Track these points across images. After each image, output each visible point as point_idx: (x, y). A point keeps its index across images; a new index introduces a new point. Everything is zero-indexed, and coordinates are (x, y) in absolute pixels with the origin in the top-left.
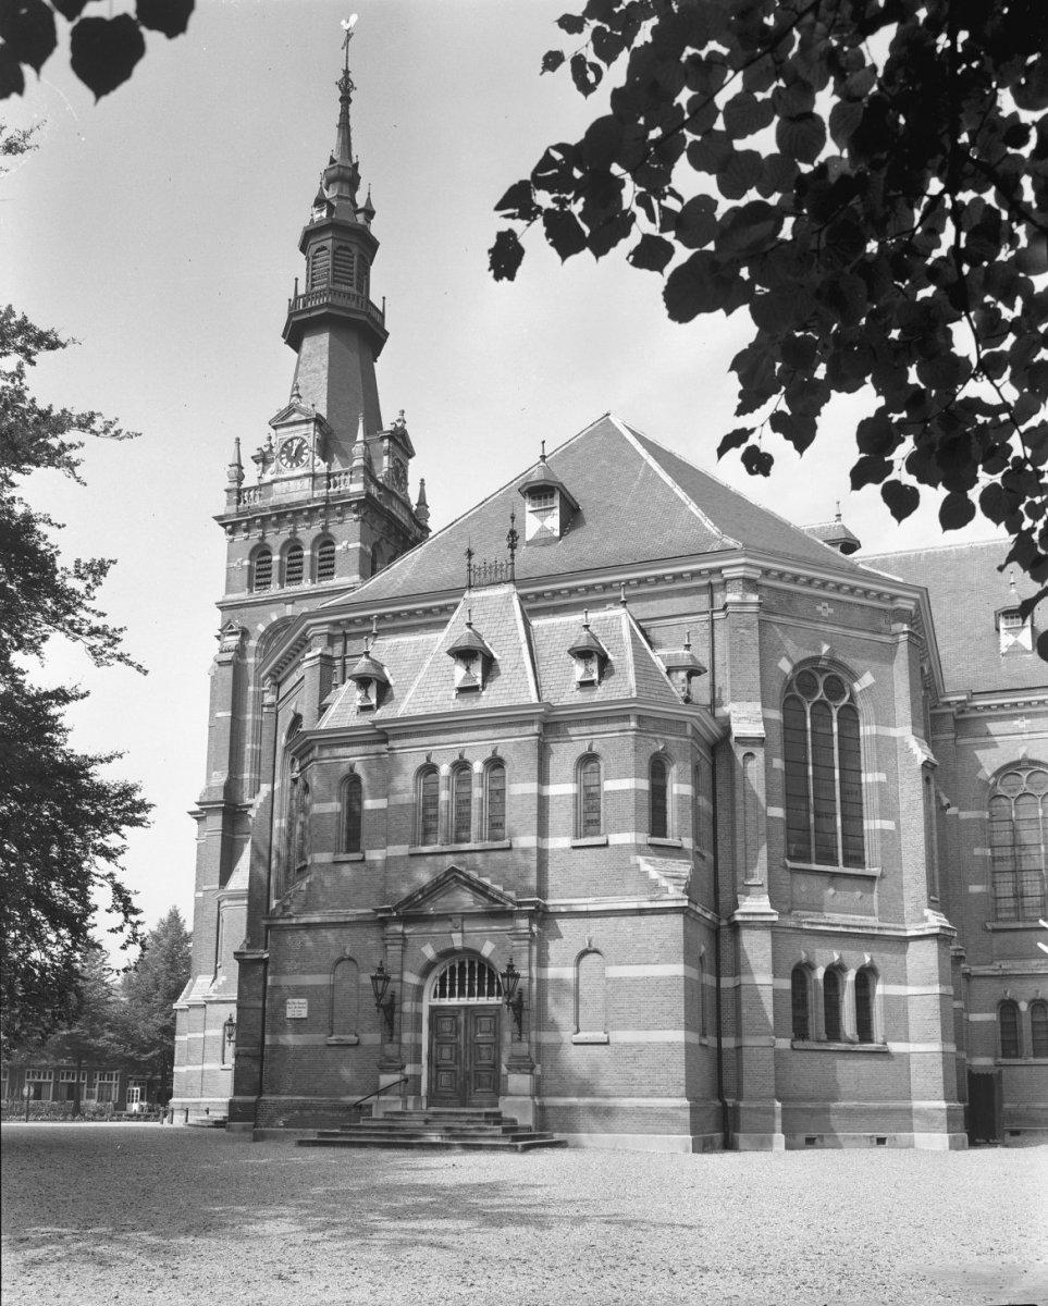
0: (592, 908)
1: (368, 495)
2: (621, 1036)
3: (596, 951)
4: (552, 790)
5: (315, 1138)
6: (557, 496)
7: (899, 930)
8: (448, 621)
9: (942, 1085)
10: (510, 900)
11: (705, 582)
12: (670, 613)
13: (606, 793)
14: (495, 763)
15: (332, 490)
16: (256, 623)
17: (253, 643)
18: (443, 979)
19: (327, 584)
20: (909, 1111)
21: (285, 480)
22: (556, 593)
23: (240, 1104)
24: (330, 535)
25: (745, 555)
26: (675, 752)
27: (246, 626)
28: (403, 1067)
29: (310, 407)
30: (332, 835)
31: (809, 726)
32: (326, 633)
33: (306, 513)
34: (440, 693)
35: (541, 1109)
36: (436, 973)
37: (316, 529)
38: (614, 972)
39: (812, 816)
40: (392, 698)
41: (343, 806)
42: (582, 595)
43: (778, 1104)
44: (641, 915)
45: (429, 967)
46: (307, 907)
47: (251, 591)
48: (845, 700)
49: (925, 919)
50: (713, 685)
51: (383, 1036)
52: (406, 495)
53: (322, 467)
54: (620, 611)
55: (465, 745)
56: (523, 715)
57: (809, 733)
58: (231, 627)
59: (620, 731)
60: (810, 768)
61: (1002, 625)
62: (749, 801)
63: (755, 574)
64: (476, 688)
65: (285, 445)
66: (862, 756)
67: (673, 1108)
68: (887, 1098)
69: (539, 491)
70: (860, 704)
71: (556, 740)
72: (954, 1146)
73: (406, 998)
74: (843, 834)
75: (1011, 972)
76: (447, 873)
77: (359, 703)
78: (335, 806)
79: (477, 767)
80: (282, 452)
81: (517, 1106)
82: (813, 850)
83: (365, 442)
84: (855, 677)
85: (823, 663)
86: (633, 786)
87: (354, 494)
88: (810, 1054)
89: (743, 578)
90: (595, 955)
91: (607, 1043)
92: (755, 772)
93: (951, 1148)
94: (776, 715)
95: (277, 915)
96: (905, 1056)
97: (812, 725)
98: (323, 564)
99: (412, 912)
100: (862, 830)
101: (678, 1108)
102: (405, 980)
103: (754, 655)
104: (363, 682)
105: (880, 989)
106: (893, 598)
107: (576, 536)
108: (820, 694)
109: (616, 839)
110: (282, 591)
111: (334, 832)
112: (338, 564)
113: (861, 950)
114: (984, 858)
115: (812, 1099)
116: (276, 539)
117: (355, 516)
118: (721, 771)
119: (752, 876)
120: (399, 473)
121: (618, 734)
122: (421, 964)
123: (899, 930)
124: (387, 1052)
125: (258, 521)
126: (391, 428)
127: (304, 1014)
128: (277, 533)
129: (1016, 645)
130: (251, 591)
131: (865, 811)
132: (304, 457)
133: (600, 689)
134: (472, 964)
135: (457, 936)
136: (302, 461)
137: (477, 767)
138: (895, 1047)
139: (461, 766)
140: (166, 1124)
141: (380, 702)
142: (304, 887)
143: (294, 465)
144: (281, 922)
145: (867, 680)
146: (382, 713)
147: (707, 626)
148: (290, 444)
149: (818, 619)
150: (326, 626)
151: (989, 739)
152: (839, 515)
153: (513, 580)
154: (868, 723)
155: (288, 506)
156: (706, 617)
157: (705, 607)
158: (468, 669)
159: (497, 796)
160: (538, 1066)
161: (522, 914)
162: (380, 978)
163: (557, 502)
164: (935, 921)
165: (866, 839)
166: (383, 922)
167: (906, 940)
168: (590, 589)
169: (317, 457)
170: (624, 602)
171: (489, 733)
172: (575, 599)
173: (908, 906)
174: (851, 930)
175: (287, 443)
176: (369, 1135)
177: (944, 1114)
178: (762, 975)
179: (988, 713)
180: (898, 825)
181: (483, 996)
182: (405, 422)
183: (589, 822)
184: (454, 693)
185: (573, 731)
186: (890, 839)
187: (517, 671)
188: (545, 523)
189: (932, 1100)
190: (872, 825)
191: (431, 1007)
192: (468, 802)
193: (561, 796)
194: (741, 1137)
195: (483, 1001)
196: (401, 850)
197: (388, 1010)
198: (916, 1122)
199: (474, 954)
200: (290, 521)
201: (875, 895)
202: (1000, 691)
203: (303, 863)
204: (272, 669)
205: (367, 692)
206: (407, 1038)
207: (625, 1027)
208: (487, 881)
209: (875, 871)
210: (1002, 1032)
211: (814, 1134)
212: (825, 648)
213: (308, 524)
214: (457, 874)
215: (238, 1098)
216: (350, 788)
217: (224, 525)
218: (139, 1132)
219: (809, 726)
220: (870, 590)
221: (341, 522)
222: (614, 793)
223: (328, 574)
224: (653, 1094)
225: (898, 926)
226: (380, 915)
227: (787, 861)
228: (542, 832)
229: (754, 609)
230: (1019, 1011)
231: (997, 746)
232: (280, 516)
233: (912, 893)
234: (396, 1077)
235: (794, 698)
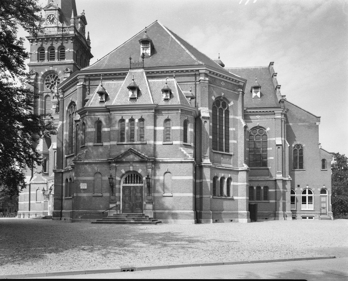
0: (168, 161)
1: (75, 35)
2: (175, 195)
3: (169, 172)
4: (157, 128)
5: (96, 221)
6: (150, 44)
7: (237, 168)
8: (125, 78)
9: (246, 207)
10: (147, 158)
11: (194, 73)
12: (184, 81)
13: (172, 130)
14: (142, 120)
15: (64, 32)
16: (41, 71)
17: (40, 78)
18: (126, 179)
19: (63, 61)
20: (238, 213)
21: (49, 27)
22: (153, 72)
23: (56, 212)
24: (64, 46)
25: (206, 67)
26: (189, 119)
27: (37, 72)
28: (116, 202)
29: (56, 5)
30: (93, 138)
31: (218, 114)
32: (84, 78)
33: (56, 39)
34: (125, 99)
35: (155, 213)
36: (125, 177)
37: (59, 44)
38: (174, 178)
39: (218, 139)
40: (109, 99)
41: (96, 129)
42: (165, 74)
43: (211, 212)
44: (181, 163)
45: (123, 175)
46: (86, 158)
47: (38, 61)
48: (226, 109)
50: (196, 102)
52: (85, 36)
53: (60, 25)
54: (174, 80)
55: (133, 114)
56: (151, 107)
57: (218, 116)
58: (33, 72)
59: (176, 113)
60: (218, 126)
61: (253, 90)
62: (205, 134)
63: (208, 72)
64: (135, 98)
65: (48, 16)
66: (230, 123)
67: (189, 213)
68: (233, 210)
69: (145, 42)
70: (230, 110)
71: (158, 114)
72: (248, 222)
73: (117, 184)
74: (225, 144)
75: (253, 179)
76: (129, 150)
77: (100, 100)
79: (137, 121)
80: (47, 18)
81: (149, 210)
82: (218, 147)
83: (74, 19)
84: (229, 102)
85: (222, 98)
86: (180, 129)
87: (71, 35)
88: (217, 199)
89: (204, 73)
90: (169, 173)
91: (172, 196)
92: (207, 126)
93: (248, 222)
94: (211, 111)
95: (77, 160)
96: (237, 200)
97: (219, 114)
98: (61, 55)
99: (118, 160)
100: (229, 143)
101: (191, 213)
102: (116, 179)
103: (207, 94)
104: (101, 94)
105: (232, 183)
106: (239, 82)
107: (155, 56)
108: (221, 106)
109: (175, 142)
110: (48, 62)
111: (94, 136)
112: (66, 55)
113: (228, 174)
115: (217, 211)
116: (46, 46)
117: (71, 41)
118: (198, 126)
119: (206, 154)
120: (83, 29)
121: (176, 114)
122: (121, 175)
123: (237, 168)
124: (111, 198)
125: (40, 40)
126: (81, 15)
127: (86, 188)
128: (46, 44)
129: (256, 96)
130: (38, 61)
131: (230, 138)
132: (55, 21)
133: (170, 101)
134: (134, 175)
135: (131, 167)
136: (54, 22)
137: (137, 121)
138: (235, 198)
139: (132, 120)
140: (17, 218)
141: (106, 100)
142: (85, 152)
143: (52, 23)
144: (78, 162)
145: (232, 103)
146: (106, 104)
147: (194, 85)
148: (50, 16)
149: (221, 86)
150: (84, 76)
151: (250, 120)
152: (219, 57)
153: (143, 68)
154: (232, 115)
155: (50, 36)
156: (194, 83)
157: (194, 80)
158: (133, 93)
159: (142, 129)
160: (154, 202)
161: (149, 162)
162: (111, 178)
163: (150, 46)
164: (246, 167)
165: (230, 145)
166: (110, 163)
167: (238, 171)
168: (163, 72)
169: (59, 21)
170: (174, 77)
171: (140, 111)
172: (163, 74)
173: (239, 163)
174: (227, 168)
175: (49, 15)
176: (112, 220)
177: (246, 214)
178: (208, 180)
179: (250, 113)
180: (237, 141)
181: (138, 183)
182: (84, 14)
183: (167, 138)
184: (129, 99)
185: (163, 112)
186: (235, 145)
187: (147, 94)
188: (146, 51)
189: (243, 210)
190: (231, 141)
191: (123, 186)
192: (134, 130)
193: (160, 130)
194: (202, 220)
195: (138, 185)
196: (115, 143)
197: (112, 187)
198: (239, 216)
200: (51, 41)
201: (232, 159)
202: (253, 108)
203: (84, 145)
204: (63, 87)
205: (102, 97)
206: (117, 194)
207: (177, 192)
208: (139, 152)
209: (232, 153)
210: (264, 194)
211: (217, 219)
212: (223, 94)
213: (56, 42)
214: (132, 150)
215: (55, 211)
216: (98, 124)
217: (29, 40)
218: (3, 223)
219: (218, 114)
220: (231, 78)
221: (67, 43)
222: (174, 130)
223: (53, 59)
224: (184, 209)
225: (236, 167)
226: (109, 161)
227: (213, 150)
228: (155, 140)
229: (207, 82)
230: (261, 189)
231: (252, 122)
232: (48, 39)
233: (240, 160)
234: (114, 205)
235: (215, 107)
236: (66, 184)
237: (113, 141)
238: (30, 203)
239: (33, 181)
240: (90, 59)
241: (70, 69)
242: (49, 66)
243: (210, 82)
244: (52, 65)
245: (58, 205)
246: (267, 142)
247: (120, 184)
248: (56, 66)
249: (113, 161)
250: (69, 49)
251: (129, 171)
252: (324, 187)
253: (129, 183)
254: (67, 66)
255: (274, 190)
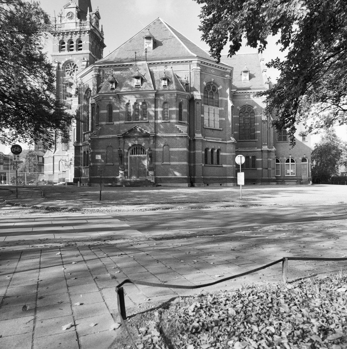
6: (152, 39)
18: (132, 151)
26: (184, 102)
36: (131, 149)
37: (78, 36)
45: (130, 148)
48: (216, 92)
49: (231, 139)
51: (120, 163)
78: (106, 111)
106: (227, 69)
114: (237, 126)
116: (66, 39)
134: (139, 147)
163: (152, 41)
194: (195, 184)
199: (139, 145)
232: (68, 33)
235: (206, 90)
236: (84, 156)
237: (122, 120)
238: (53, 170)
239: (57, 153)
240: (103, 48)
241: (87, 57)
242: (68, 56)
243: (201, 70)
244: (72, 55)
245: (77, 173)
246: (255, 118)
247: (127, 155)
248: (74, 56)
249: (315, 44)
250: (86, 40)
251: (135, 145)
252: (305, 156)
253: (135, 154)
254: (83, 55)
255: (261, 159)
